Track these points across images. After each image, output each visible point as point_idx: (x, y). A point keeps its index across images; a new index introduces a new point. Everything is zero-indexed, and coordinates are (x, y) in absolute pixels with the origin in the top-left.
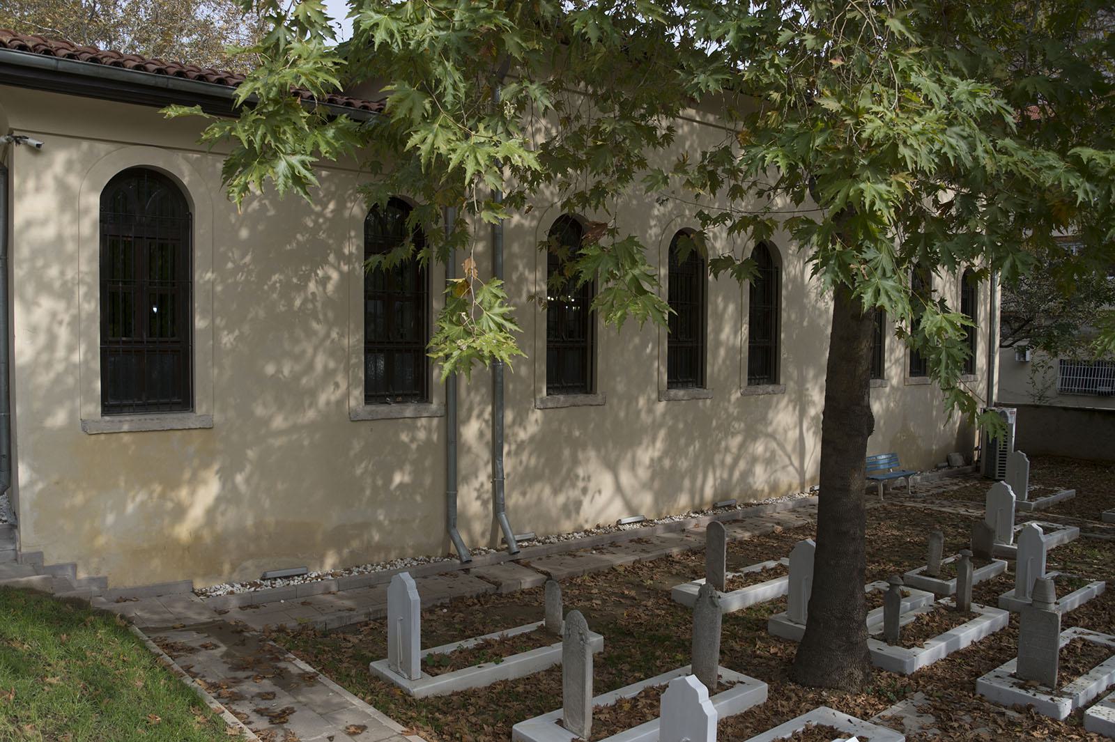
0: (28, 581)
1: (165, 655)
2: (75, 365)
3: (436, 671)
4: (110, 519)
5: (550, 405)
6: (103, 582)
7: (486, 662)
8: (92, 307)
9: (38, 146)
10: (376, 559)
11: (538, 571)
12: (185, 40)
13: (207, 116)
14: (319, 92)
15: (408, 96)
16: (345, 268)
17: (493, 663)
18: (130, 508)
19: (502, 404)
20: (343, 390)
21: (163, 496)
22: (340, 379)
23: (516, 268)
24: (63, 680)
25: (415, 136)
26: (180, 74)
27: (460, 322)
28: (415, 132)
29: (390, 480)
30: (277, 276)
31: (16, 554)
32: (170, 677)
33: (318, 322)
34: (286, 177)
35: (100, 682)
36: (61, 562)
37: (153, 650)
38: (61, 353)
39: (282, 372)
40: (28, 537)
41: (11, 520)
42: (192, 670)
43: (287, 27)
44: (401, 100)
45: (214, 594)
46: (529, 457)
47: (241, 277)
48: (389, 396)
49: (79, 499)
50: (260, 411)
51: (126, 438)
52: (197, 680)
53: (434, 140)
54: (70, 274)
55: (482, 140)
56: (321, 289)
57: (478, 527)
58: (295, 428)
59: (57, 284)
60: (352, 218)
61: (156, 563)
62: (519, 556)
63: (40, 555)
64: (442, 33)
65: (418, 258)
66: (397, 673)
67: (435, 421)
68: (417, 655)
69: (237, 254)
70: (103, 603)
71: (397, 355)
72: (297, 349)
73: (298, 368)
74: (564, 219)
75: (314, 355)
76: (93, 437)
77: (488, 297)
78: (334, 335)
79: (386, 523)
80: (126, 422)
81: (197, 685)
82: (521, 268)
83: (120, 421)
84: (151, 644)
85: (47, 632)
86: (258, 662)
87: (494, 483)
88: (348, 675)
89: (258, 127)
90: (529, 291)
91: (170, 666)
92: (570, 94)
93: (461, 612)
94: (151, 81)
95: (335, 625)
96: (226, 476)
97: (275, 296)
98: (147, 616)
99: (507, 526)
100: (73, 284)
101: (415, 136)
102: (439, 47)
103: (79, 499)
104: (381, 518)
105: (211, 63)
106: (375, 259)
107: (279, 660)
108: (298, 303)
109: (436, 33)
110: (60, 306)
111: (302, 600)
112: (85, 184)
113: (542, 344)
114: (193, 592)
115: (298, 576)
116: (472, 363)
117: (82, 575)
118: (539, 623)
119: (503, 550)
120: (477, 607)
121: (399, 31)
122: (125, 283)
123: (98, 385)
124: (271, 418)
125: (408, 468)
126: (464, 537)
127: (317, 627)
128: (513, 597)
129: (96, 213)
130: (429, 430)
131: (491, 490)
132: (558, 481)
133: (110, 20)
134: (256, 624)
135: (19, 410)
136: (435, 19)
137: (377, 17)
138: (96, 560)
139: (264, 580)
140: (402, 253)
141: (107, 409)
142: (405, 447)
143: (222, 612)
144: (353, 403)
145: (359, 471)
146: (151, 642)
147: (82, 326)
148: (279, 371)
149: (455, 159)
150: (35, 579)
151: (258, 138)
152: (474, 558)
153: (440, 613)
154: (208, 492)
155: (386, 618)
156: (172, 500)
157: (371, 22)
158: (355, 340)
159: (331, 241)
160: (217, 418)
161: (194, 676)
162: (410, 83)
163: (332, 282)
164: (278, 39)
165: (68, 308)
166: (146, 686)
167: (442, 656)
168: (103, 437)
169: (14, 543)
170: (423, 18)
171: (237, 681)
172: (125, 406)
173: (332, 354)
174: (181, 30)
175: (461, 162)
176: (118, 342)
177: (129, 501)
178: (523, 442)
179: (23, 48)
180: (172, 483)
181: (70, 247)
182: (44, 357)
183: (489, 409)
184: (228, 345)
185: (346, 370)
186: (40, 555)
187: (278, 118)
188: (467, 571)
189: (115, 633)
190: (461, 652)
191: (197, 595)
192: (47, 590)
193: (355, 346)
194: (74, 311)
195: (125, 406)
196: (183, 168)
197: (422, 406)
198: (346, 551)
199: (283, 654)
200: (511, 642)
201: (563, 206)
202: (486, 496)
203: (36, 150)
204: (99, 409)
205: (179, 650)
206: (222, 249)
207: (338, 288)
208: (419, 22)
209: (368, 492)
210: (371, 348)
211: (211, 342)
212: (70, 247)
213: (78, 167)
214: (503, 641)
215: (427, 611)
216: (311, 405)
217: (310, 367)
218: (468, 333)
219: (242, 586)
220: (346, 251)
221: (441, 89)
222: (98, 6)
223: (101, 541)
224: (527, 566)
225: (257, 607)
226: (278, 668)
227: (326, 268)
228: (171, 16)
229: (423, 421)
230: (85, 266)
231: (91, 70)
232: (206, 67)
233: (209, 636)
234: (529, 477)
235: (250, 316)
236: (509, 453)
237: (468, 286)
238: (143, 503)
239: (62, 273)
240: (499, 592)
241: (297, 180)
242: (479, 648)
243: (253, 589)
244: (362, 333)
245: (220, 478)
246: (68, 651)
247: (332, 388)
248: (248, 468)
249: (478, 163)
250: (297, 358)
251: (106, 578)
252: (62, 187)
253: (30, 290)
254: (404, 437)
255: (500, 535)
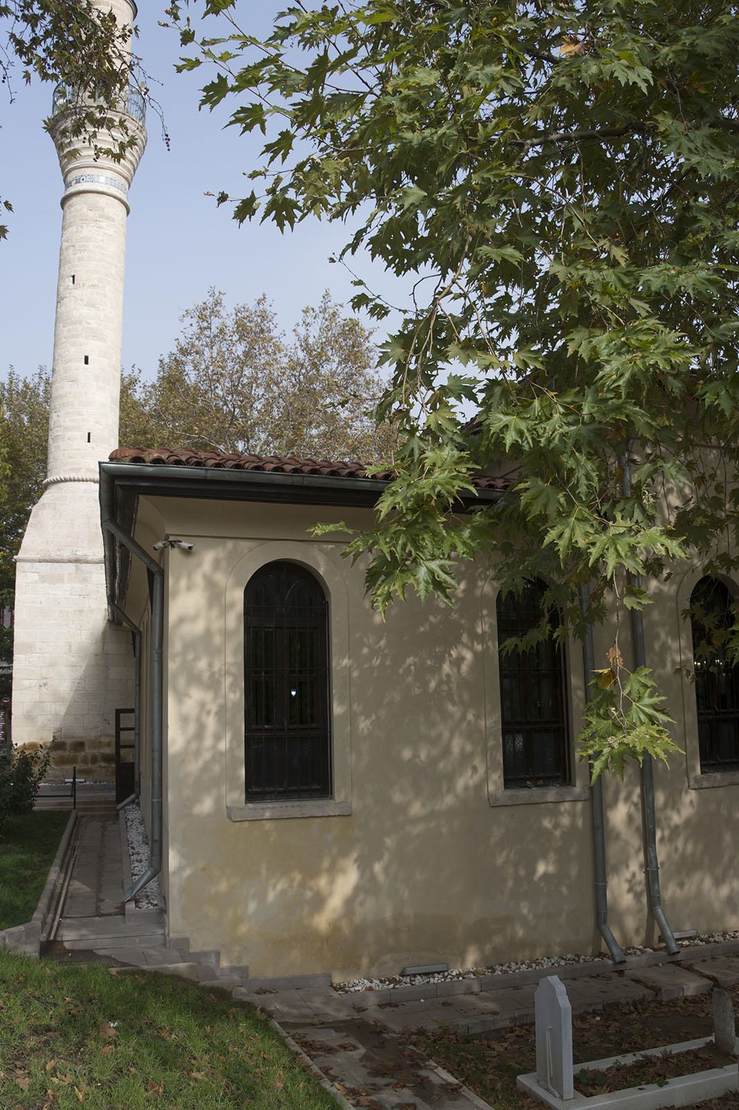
0: (176, 968)
1: (304, 1055)
2: (221, 754)
3: (591, 1090)
4: (252, 907)
5: (705, 784)
6: (243, 971)
7: (648, 1083)
8: (236, 696)
9: (190, 548)
10: (520, 957)
11: (702, 975)
12: (314, 432)
13: (350, 532)
14: (455, 499)
15: (541, 492)
16: (479, 647)
17: (656, 1085)
18: (271, 896)
19: (652, 786)
20: (481, 775)
21: (303, 885)
22: (477, 762)
23: (658, 636)
24: (207, 1075)
25: (552, 532)
26: (314, 471)
27: (607, 716)
28: (552, 527)
29: (534, 870)
30: (411, 658)
31: (165, 939)
32: (309, 1079)
33: (454, 704)
34: (427, 582)
35: (241, 1081)
36: (206, 949)
37: (292, 1048)
38: (208, 742)
39: (419, 757)
40: (175, 919)
41: (161, 905)
42: (330, 1072)
43: (420, 437)
44: (535, 498)
45: (352, 989)
46: (685, 843)
47: (376, 662)
48: (529, 779)
49: (223, 886)
50: (397, 797)
51: (268, 826)
52: (336, 1084)
53: (571, 533)
54: (217, 666)
55: (622, 530)
56: (455, 670)
57: (631, 923)
58: (432, 815)
59: (206, 676)
60: (484, 596)
61: (295, 955)
62: (679, 957)
63: (186, 941)
64: (572, 428)
65: (555, 636)
66: (547, 1090)
67: (579, 806)
68: (569, 1070)
69: (371, 640)
70: (244, 994)
71: (537, 737)
72: (433, 733)
73: (435, 752)
74: (705, 580)
75: (451, 738)
76: (237, 824)
77: (636, 686)
78: (470, 717)
79: (530, 917)
80: (268, 809)
81: (335, 1089)
82: (663, 636)
83: (263, 809)
84: (290, 1041)
85: (193, 1023)
86: (398, 1068)
87: (647, 873)
88: (493, 1089)
89: (399, 537)
90: (674, 662)
91: (309, 1066)
92: (702, 449)
93: (615, 1020)
94: (289, 481)
95: (478, 1030)
96: (364, 865)
97: (410, 679)
98: (286, 1009)
99: (664, 922)
100: (220, 675)
101: (552, 532)
102: (570, 442)
103: (223, 886)
104: (525, 911)
105: (339, 455)
106: (511, 642)
107: (421, 1068)
108: (433, 685)
109: (566, 429)
110: (208, 696)
111: (443, 1000)
112: (230, 581)
113: (692, 717)
114: (331, 986)
115: (439, 973)
116: (624, 761)
117: (224, 963)
118: (708, 1039)
119: (661, 949)
120: (634, 1016)
121: (528, 430)
122: (266, 672)
123: (242, 772)
124: (409, 804)
125: (552, 856)
126: (616, 934)
127: (459, 1031)
128: (675, 1005)
129: (240, 607)
130: (573, 815)
131: (644, 881)
132: (719, 871)
133: (247, 422)
134: (395, 1025)
135: (171, 797)
136: (563, 414)
137: (505, 419)
138: (238, 948)
139: (403, 976)
140: (538, 635)
141: (251, 796)
142: (549, 833)
143: (361, 1010)
144: (491, 787)
145: (500, 860)
146: (290, 1039)
147: (228, 715)
148: (416, 755)
149: (595, 552)
150: (182, 966)
151: (399, 548)
152: (629, 959)
153: (593, 1021)
154: (347, 881)
155: (533, 1024)
156: (311, 889)
157: (501, 424)
158: (492, 721)
159: (463, 621)
160: (356, 805)
161: (333, 1079)
162: (542, 478)
163: (465, 662)
164: (413, 450)
165: (215, 698)
166: (285, 1088)
167: (597, 1073)
168: (246, 824)
169: (164, 927)
170: (551, 415)
171: (376, 1088)
172: (267, 793)
173: (468, 737)
174: (310, 423)
175: (602, 556)
176: (261, 730)
177: (270, 889)
178: (677, 827)
179: (178, 462)
180: (311, 872)
181: (217, 640)
182: (194, 746)
183: (638, 791)
184: (365, 730)
185: (484, 752)
186: (186, 941)
187: (417, 526)
188: (621, 973)
189: (256, 1028)
190: (618, 1070)
191: (336, 989)
192: (193, 978)
193: (491, 728)
194: (220, 701)
195: (267, 793)
196: (320, 561)
197: (564, 790)
198: (488, 947)
199: (424, 1060)
200: (675, 1061)
201: (705, 569)
202: (639, 888)
203: (188, 552)
204: (243, 797)
205: (318, 1049)
206: (357, 635)
207: (473, 668)
208: (548, 419)
209: (510, 883)
210: (508, 729)
211: (349, 728)
212: (217, 640)
213: (223, 564)
214: (667, 1058)
215: (579, 1018)
216: (449, 791)
217: (447, 751)
218: (619, 727)
219: (381, 981)
220: (479, 630)
221: (574, 481)
222: (237, 410)
223: (243, 929)
224: (689, 968)
225: (396, 1006)
226: (419, 1076)
227: (460, 647)
228: (302, 412)
229: (566, 806)
230: (232, 658)
231: (236, 475)
232: (335, 458)
233: (347, 1036)
234: (686, 866)
235: (386, 701)
236: (662, 839)
237: (614, 677)
238: (283, 892)
239: (210, 665)
240: (658, 998)
241: (438, 585)
242: (639, 1066)
243: (392, 986)
244: (499, 714)
245: (358, 867)
246: (211, 1044)
247: (470, 772)
248: (386, 857)
249: (619, 555)
250: (434, 742)
251: (247, 968)
252: (210, 584)
253: (182, 682)
254: (547, 823)
255: (657, 933)
